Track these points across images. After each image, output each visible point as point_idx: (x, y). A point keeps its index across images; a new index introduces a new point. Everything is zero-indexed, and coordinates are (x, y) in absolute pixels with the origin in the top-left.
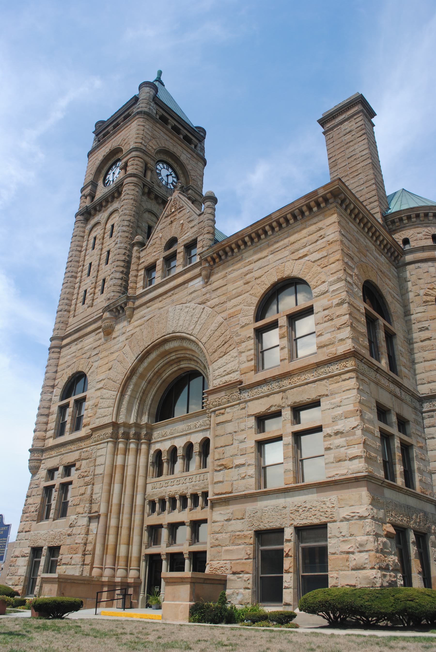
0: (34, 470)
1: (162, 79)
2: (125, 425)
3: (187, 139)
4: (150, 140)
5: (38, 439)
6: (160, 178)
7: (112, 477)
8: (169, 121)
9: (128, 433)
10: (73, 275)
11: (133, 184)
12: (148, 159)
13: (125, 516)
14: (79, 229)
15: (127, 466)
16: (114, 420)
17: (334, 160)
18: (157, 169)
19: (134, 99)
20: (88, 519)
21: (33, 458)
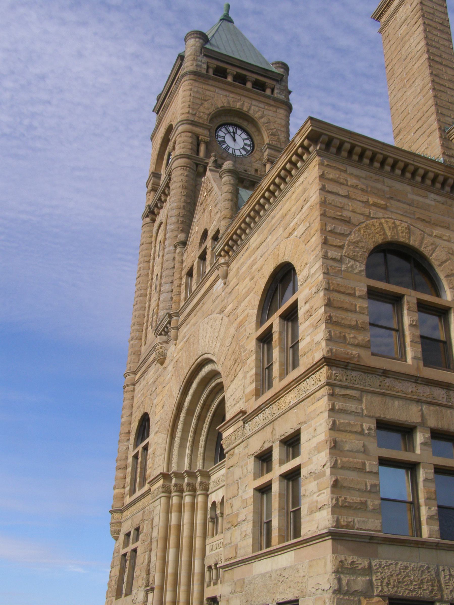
0: (116, 535)
1: (230, 15)
2: (179, 475)
3: (260, 86)
4: (202, 104)
5: (116, 498)
6: (224, 146)
7: (166, 540)
8: (228, 71)
9: (169, 487)
10: (142, 294)
11: (180, 168)
12: (198, 130)
13: (182, 588)
14: (145, 235)
15: (183, 525)
16: (165, 471)
17: (390, 67)
18: (219, 136)
19: (179, 59)
20: (145, 594)
21: (113, 521)
